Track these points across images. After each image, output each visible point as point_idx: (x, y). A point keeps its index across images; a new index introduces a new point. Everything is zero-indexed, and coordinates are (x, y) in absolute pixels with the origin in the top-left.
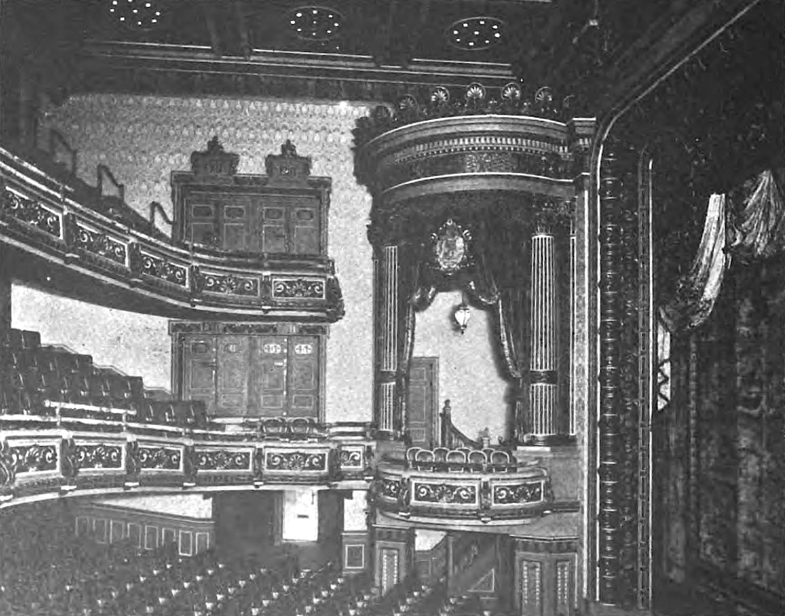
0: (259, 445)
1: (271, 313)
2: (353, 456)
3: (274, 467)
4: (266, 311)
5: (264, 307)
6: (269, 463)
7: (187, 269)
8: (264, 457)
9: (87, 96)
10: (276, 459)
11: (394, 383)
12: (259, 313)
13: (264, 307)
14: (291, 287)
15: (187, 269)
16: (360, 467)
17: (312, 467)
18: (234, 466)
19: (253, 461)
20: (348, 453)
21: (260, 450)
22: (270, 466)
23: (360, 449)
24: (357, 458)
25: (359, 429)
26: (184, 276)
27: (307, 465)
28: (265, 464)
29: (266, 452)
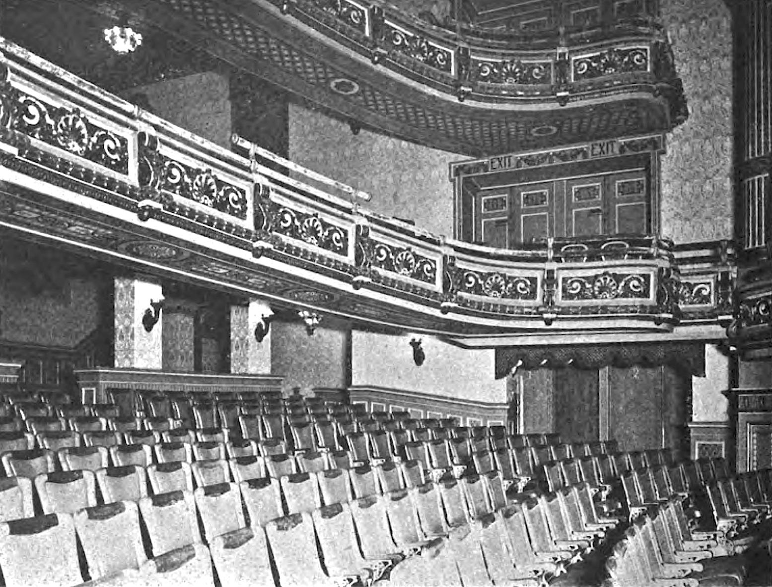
0: (548, 266)
1: (555, 325)
2: (699, 291)
3: (571, 297)
4: (549, 322)
5: (545, 316)
6: (564, 290)
7: (452, 52)
8: (556, 282)
9: (215, 353)
10: (575, 285)
11: (767, 175)
12: (541, 325)
13: (545, 316)
14: (593, 284)
15: (452, 52)
16: (712, 304)
17: (627, 293)
18: (515, 294)
19: (542, 286)
20: (690, 287)
21: (551, 272)
22: (567, 295)
23: (710, 279)
24: (705, 293)
25: (706, 253)
26: (448, 60)
27: (620, 291)
28: (559, 292)
29: (560, 275)
